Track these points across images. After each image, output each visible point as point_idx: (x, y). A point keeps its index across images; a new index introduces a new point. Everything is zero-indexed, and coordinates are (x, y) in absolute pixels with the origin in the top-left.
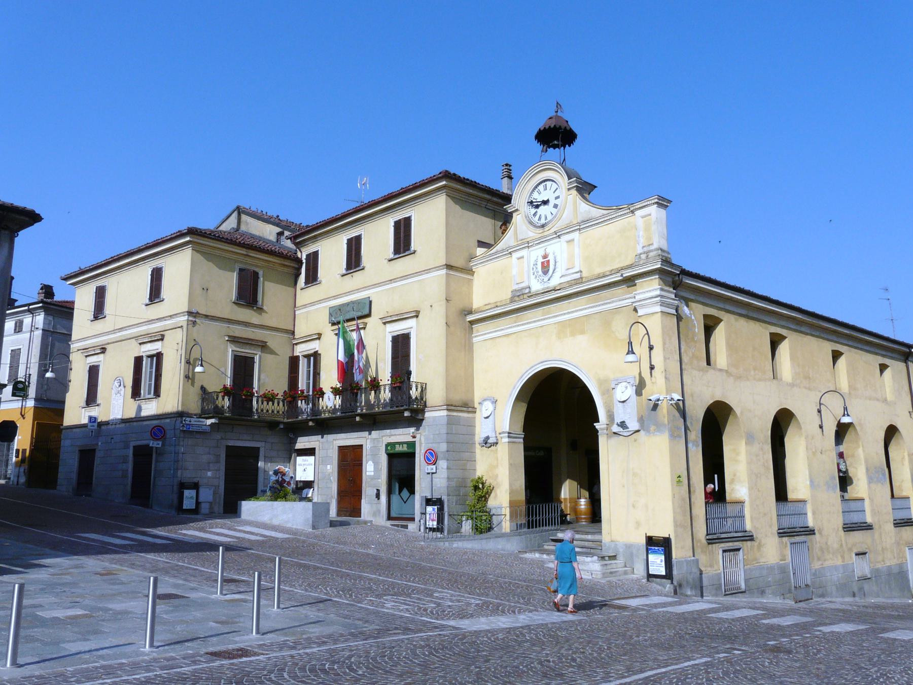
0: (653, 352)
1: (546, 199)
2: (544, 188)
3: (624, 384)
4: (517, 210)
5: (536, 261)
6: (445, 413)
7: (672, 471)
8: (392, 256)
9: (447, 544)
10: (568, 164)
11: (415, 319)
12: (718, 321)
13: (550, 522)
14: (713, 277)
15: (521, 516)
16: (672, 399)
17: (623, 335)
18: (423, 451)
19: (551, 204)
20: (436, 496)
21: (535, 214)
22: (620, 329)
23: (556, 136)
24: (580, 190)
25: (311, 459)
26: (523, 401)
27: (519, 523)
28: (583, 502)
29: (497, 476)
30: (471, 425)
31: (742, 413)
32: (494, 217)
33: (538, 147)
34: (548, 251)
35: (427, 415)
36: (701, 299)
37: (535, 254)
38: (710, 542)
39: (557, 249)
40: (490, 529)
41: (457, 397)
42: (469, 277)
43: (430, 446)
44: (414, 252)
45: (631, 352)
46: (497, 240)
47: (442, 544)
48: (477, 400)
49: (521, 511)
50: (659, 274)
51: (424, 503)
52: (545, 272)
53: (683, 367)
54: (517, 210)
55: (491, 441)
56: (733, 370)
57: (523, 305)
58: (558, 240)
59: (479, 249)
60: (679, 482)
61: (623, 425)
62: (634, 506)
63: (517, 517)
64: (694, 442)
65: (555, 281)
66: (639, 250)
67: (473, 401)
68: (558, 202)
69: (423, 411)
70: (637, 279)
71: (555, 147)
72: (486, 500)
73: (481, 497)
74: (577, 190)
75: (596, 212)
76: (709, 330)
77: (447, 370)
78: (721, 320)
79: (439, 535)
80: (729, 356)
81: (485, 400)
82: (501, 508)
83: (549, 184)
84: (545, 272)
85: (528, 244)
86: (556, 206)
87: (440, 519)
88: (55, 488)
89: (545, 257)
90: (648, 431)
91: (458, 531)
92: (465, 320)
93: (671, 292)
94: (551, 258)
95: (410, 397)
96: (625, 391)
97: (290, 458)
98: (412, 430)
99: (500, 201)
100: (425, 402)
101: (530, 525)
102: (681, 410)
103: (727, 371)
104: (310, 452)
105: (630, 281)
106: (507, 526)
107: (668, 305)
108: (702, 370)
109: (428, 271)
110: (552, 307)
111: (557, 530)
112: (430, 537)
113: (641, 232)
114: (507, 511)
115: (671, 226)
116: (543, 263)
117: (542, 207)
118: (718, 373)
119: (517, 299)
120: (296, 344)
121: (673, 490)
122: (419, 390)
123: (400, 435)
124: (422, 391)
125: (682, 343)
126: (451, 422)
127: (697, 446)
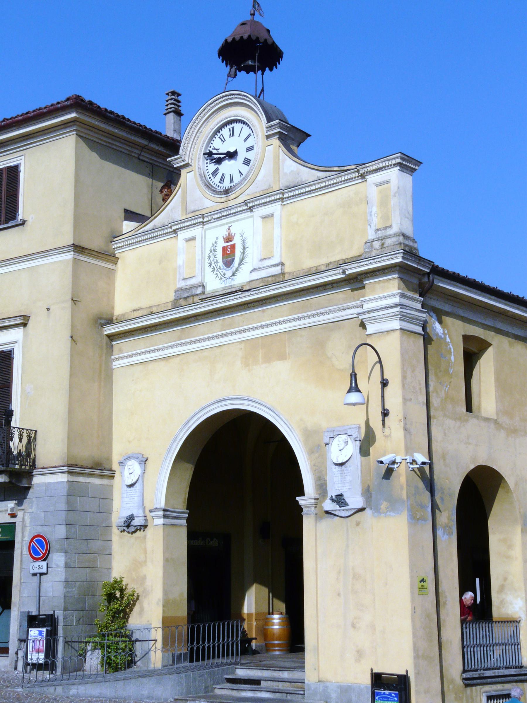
0: (387, 389)
1: (232, 150)
2: (230, 131)
3: (344, 437)
4: (187, 165)
5: (215, 245)
6: (64, 478)
7: (411, 571)
9: (59, 689)
10: (269, 98)
11: (20, 330)
12: (484, 345)
13: (224, 652)
14: (479, 279)
15: (180, 642)
16: (414, 462)
17: (344, 363)
18: (27, 539)
19: (241, 158)
20: (46, 610)
21: (215, 173)
22: (339, 352)
23: (250, 52)
24: (283, 138)
26: (189, 462)
27: (177, 653)
28: (276, 618)
29: (144, 578)
30: (106, 497)
31: (516, 484)
32: (152, 175)
33: (223, 69)
34: (233, 231)
35: (36, 480)
36: (461, 312)
37: (214, 235)
38: (469, 683)
39: (247, 228)
40: (131, 663)
41: (86, 453)
42: (110, 266)
43: (39, 530)
44: (23, 223)
45: (354, 388)
46: (155, 211)
47: (52, 689)
48: (116, 458)
49: (180, 634)
50: (400, 272)
51: (25, 624)
52: (228, 263)
53: (432, 413)
54: (187, 165)
55: (137, 522)
56: (504, 420)
57: (192, 312)
58: (249, 214)
59: (126, 223)
60: (422, 588)
61: (339, 500)
62: (354, 626)
63: (173, 644)
64: (446, 527)
65: (242, 278)
66: (371, 235)
67: (109, 459)
68: (250, 155)
69: (29, 475)
70: (367, 278)
71: (249, 69)
72: (126, 617)
73: (118, 612)
74: (280, 139)
75: (307, 174)
76: (471, 358)
77: (71, 411)
78: (489, 345)
79: (47, 675)
80: (499, 399)
81: (128, 458)
82: (149, 629)
83: (237, 127)
84: (228, 263)
85: (202, 219)
86: (247, 162)
87: (51, 649)
89: (228, 239)
90: (377, 510)
91: (79, 667)
92: (100, 333)
93: (417, 301)
94: (237, 241)
95: (9, 452)
96: (343, 449)
98: (11, 504)
99: (161, 149)
100: (34, 461)
101: (195, 655)
102: (427, 477)
103: (496, 422)
105: (356, 282)
106: (157, 658)
107: (411, 320)
108: (460, 419)
109: (44, 253)
110: (237, 316)
111: (236, 664)
112: (33, 678)
113: (374, 208)
114: (158, 635)
115: (419, 199)
116: (224, 249)
117: (226, 163)
118: (483, 424)
119: (182, 302)
121: (413, 600)
122: (25, 440)
124: (29, 442)
125: (431, 377)
126: (73, 492)
127: (450, 534)
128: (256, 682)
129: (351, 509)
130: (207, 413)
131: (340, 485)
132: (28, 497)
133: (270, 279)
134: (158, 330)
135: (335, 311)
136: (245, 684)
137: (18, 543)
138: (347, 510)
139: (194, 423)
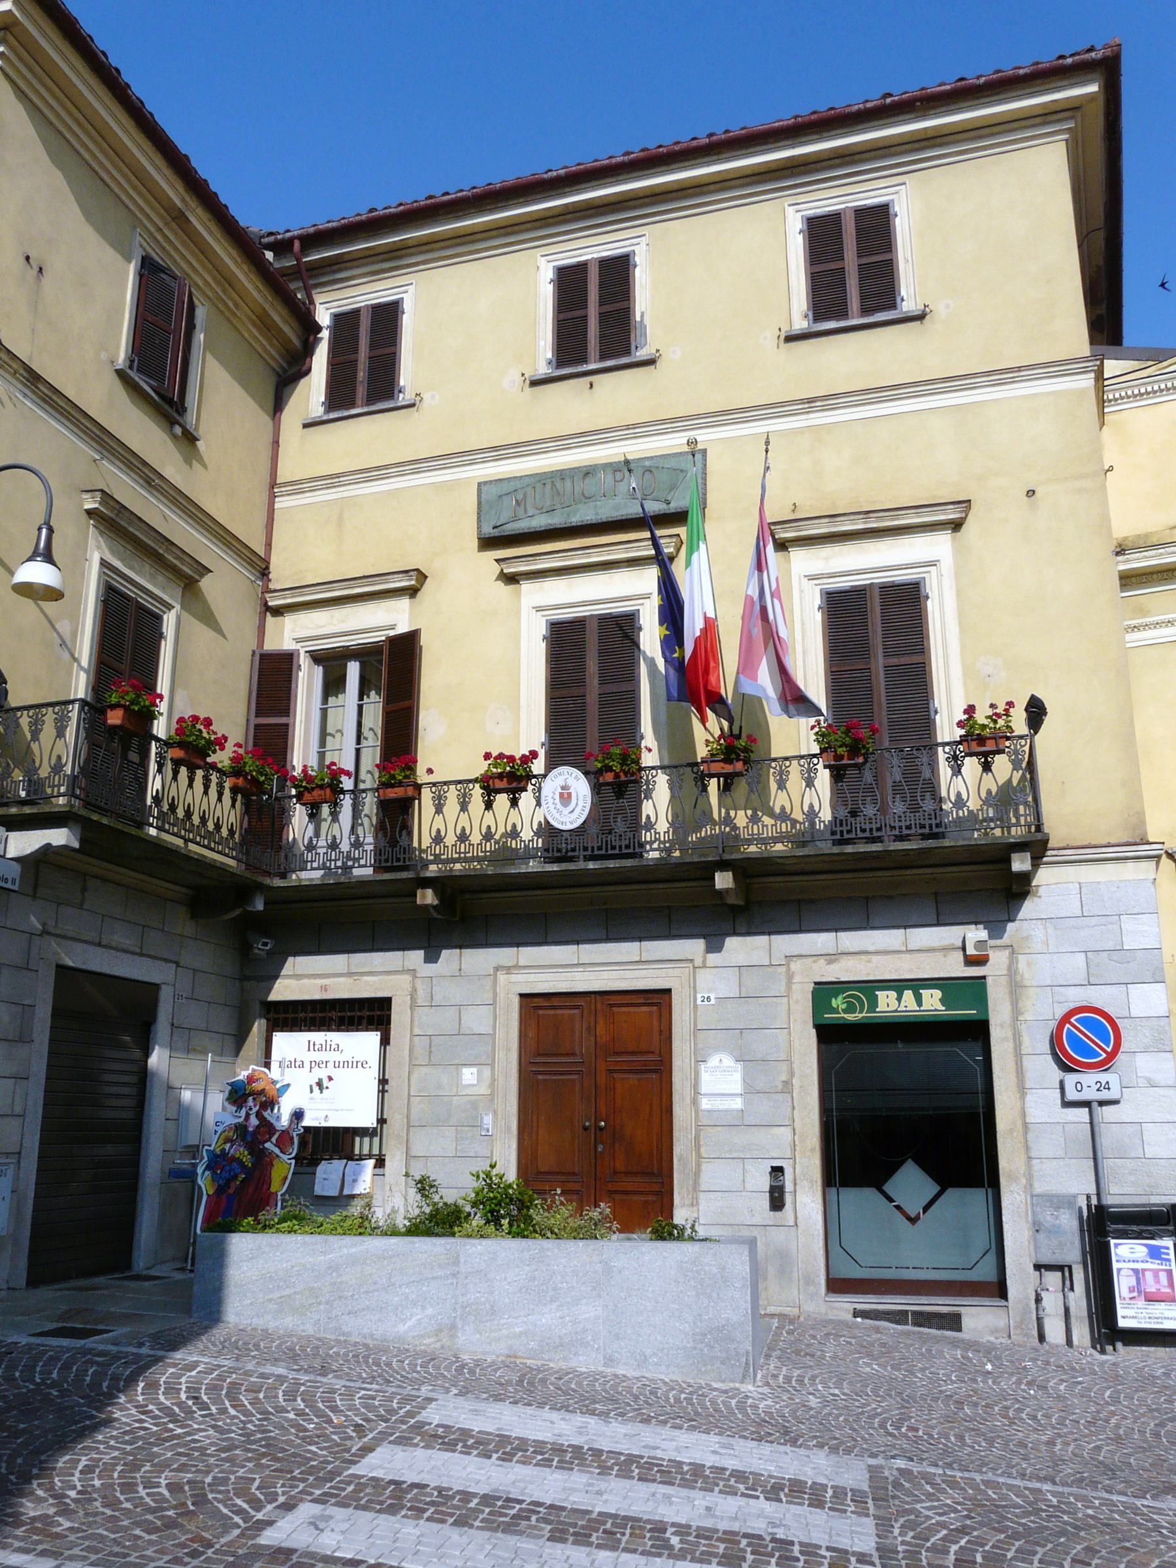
11: (404, 603)
25: (366, 1043)
97: (240, 1038)
98: (975, 934)
104: (370, 1014)
120: (278, 611)
123: (901, 959)
132: (1020, 916)
137: (1002, 1026)
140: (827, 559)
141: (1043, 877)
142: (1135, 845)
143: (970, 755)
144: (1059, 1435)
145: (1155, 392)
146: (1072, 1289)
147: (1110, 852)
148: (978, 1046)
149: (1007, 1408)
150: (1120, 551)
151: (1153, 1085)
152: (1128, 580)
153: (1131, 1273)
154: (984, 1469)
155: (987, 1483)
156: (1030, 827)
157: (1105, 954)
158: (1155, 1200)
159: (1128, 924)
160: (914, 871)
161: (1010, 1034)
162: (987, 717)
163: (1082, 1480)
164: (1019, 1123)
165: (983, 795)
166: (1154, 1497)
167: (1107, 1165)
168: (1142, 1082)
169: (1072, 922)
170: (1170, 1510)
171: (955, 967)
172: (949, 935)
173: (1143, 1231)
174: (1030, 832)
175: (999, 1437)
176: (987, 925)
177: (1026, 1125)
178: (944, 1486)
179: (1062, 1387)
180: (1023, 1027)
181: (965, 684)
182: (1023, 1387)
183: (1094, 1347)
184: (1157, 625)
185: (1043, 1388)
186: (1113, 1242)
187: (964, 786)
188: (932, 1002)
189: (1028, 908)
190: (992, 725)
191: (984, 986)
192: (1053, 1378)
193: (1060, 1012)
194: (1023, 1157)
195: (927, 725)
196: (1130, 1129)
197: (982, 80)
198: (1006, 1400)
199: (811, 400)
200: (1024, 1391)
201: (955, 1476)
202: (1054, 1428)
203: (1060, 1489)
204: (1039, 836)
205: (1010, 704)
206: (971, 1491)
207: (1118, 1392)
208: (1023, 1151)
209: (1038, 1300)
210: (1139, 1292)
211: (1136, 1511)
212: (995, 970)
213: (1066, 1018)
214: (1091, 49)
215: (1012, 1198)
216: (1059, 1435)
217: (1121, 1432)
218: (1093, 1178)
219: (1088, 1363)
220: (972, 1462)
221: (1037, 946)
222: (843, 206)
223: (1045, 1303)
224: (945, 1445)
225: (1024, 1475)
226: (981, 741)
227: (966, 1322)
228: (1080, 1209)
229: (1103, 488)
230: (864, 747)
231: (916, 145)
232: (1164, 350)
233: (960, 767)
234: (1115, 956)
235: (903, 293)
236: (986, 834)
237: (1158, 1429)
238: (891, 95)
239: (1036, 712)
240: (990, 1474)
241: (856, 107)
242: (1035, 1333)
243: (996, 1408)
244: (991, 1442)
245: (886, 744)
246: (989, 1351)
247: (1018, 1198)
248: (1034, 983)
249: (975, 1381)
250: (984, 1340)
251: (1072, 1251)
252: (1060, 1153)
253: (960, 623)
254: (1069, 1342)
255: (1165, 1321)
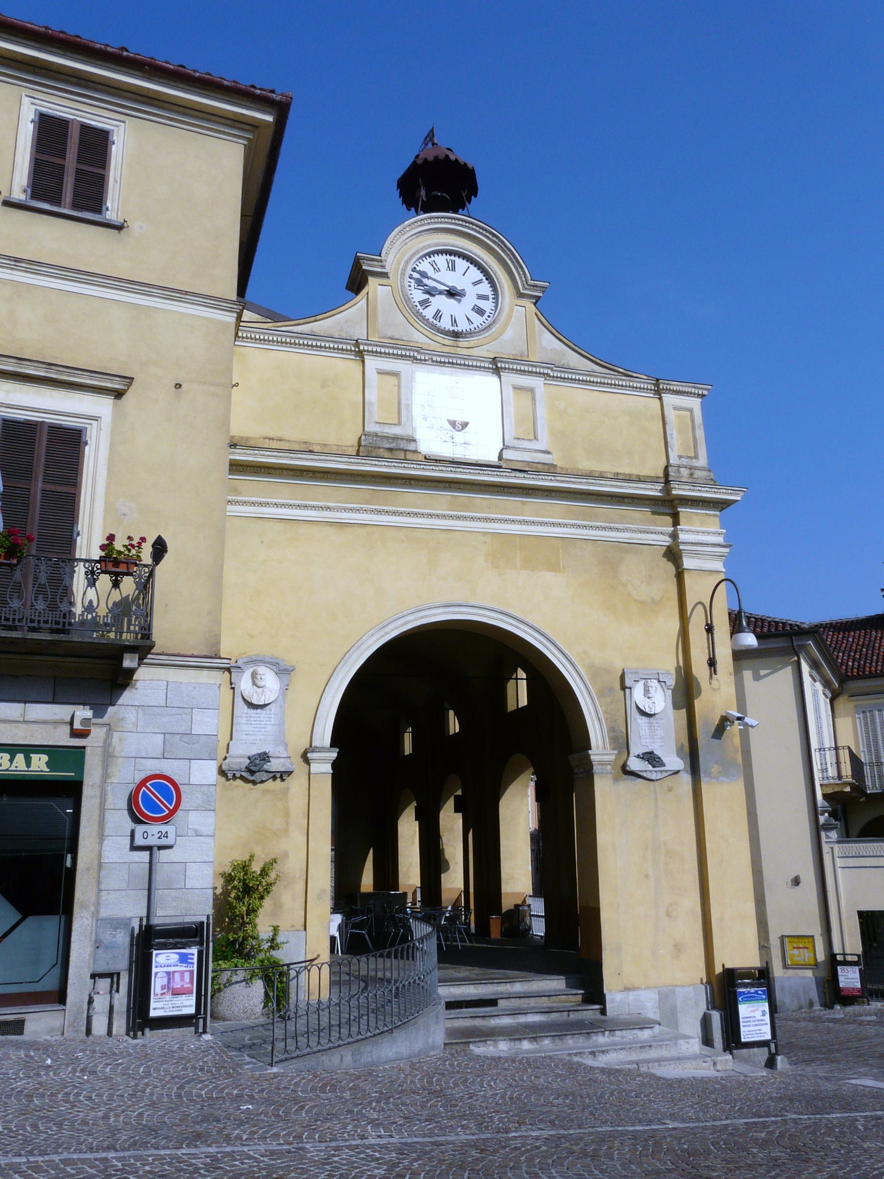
8: (19, 195)
54: (385, 275)
55: (275, 765)
88: (21, 1033)
98: (83, 713)
128: (493, 1002)
129: (666, 771)
130: (422, 617)
131: (648, 740)
132: (120, 702)
133: (540, 466)
134: (410, 486)
135: (632, 531)
136: (466, 1007)
138: (661, 772)
139: (396, 628)
140: (8, 392)
141: (143, 674)
142: (211, 658)
143: (105, 572)
144: (111, 1110)
145: (269, 341)
146: (118, 991)
147: (193, 661)
148: (70, 801)
149: (68, 1094)
150: (233, 445)
151: (198, 834)
152: (237, 467)
153: (165, 975)
154: (60, 1150)
155: (65, 1162)
156: (137, 634)
157: (178, 736)
158: (188, 919)
159: (197, 715)
160: (40, 658)
161: (98, 793)
162: (125, 546)
163: (135, 1143)
164: (96, 862)
165: (110, 605)
166: (188, 1146)
167: (158, 894)
168: (191, 832)
169: (157, 710)
170: (202, 1153)
171: (62, 738)
172: (62, 711)
173: (177, 943)
174: (136, 638)
175: (65, 1120)
176: (93, 706)
177: (100, 865)
178: (30, 1172)
179: (108, 1070)
180: (109, 788)
181: (105, 518)
182: (78, 1074)
183: (128, 1034)
184: (244, 503)
185: (93, 1072)
186: (155, 952)
187: (90, 595)
188: (40, 764)
189: (127, 697)
190: (126, 552)
191: (83, 754)
192: (100, 1063)
193: (138, 780)
194: (95, 889)
195: (70, 543)
196: (178, 867)
197: (198, 75)
198: (66, 1087)
199: (17, 260)
200: (79, 1077)
201: (37, 1162)
202: (106, 1104)
203: (121, 1154)
204: (148, 643)
205: (143, 539)
206: (53, 1172)
207: (149, 1067)
208: (95, 885)
209: (90, 1001)
210: (169, 989)
211: (179, 1160)
212: (93, 743)
213: (143, 783)
214: (273, 92)
215: (82, 923)
216: (111, 1110)
217: (155, 1098)
218: (146, 905)
219: (125, 1047)
220: (49, 1146)
221: (129, 726)
222: (72, 117)
223: (95, 1004)
224: (23, 1135)
225: (92, 1148)
226: (114, 562)
227: (29, 1027)
228: (133, 929)
229: (230, 397)
230: (20, 551)
231: (139, 98)
232: (280, 315)
233: (95, 581)
234: (185, 738)
235: (109, 204)
236: (103, 635)
237: (180, 1091)
238: (127, 51)
239: (160, 549)
240: (65, 1153)
241: (98, 46)
242: (84, 1028)
243: (60, 1096)
244: (60, 1125)
245: (34, 552)
246: (46, 1048)
247: (87, 922)
248: (123, 754)
249: (38, 1075)
250: (42, 1040)
251: (121, 962)
252: (124, 886)
253: (109, 470)
254: (110, 1033)
255: (183, 1009)
